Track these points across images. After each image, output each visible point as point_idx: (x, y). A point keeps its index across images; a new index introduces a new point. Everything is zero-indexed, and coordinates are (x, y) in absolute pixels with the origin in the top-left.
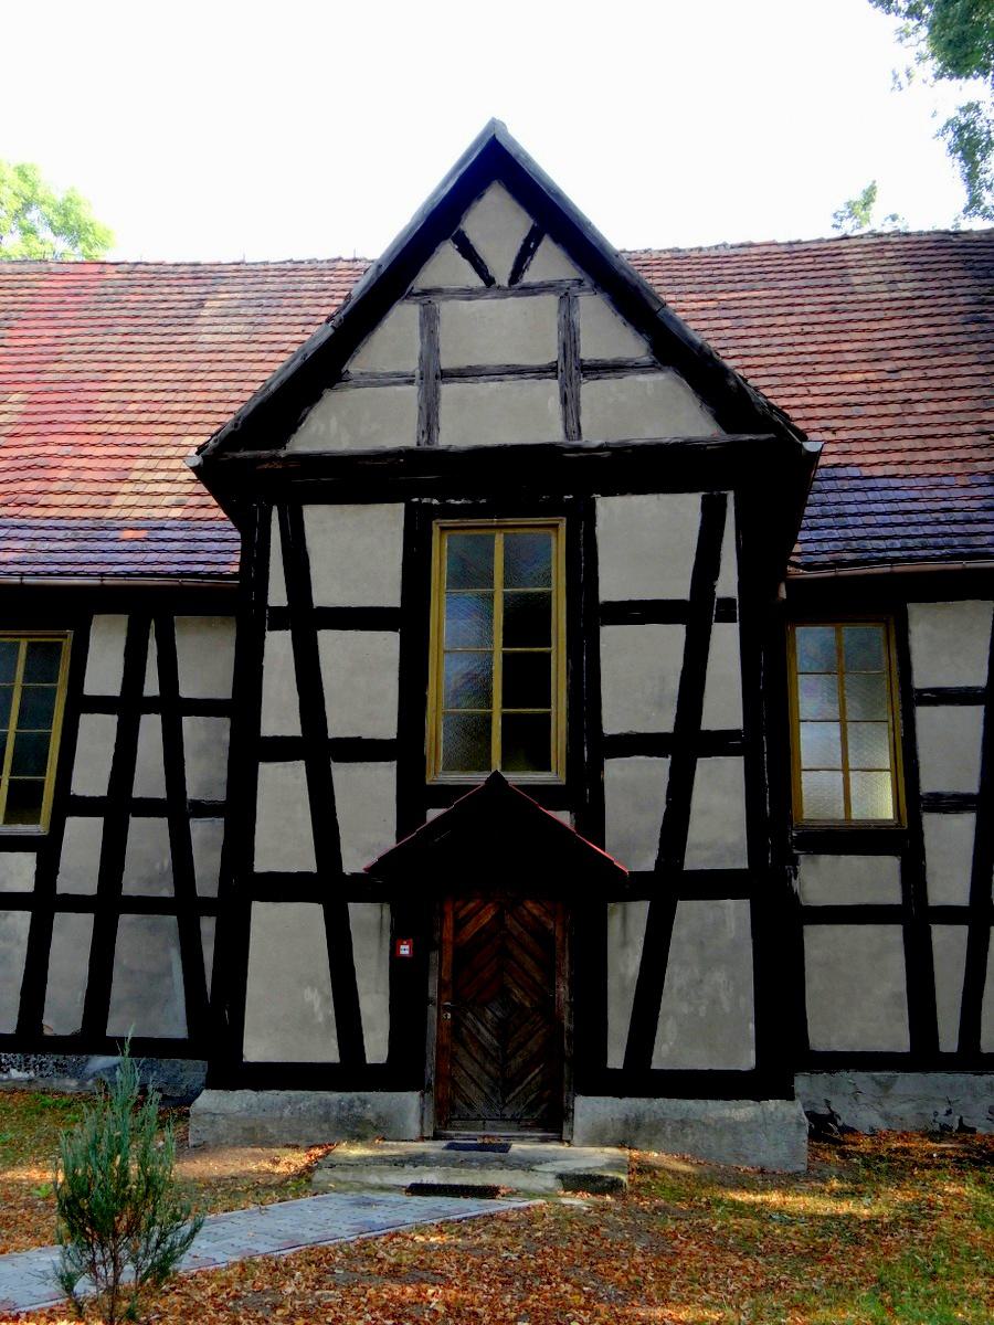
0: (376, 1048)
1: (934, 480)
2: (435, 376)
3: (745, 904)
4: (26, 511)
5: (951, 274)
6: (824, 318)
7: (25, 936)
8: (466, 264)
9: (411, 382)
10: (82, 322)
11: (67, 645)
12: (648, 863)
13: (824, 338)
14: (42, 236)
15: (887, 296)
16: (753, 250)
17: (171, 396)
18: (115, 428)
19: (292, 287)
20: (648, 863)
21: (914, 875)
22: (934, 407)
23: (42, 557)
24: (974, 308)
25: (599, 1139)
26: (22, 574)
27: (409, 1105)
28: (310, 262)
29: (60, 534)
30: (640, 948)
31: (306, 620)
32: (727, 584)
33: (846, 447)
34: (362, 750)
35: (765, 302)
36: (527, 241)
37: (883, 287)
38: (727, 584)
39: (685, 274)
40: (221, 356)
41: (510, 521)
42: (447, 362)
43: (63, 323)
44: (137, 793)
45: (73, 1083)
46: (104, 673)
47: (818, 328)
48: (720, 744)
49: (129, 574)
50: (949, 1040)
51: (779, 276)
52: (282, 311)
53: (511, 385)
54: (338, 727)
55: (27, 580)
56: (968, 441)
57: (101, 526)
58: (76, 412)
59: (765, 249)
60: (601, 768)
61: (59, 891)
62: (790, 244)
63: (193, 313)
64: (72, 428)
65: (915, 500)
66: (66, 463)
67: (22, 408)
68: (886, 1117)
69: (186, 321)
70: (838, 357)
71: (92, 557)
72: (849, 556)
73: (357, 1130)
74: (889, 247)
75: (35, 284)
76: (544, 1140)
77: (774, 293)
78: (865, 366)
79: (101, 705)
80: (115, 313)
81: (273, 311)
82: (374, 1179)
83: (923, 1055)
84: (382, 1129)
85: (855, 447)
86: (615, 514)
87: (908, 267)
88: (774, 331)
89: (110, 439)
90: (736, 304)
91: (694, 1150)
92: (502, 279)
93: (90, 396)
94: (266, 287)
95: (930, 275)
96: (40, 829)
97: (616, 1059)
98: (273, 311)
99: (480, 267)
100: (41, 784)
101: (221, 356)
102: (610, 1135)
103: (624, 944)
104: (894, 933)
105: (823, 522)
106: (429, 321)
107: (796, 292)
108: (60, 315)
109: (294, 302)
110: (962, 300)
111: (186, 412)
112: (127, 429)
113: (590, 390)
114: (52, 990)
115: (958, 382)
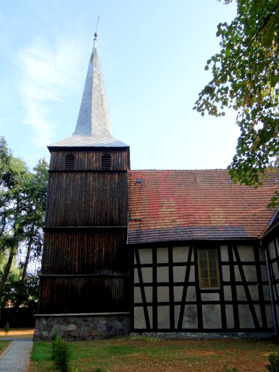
21: (222, 296)
45: (236, 338)
46: (225, 257)
50: (176, 327)
55: (211, 239)
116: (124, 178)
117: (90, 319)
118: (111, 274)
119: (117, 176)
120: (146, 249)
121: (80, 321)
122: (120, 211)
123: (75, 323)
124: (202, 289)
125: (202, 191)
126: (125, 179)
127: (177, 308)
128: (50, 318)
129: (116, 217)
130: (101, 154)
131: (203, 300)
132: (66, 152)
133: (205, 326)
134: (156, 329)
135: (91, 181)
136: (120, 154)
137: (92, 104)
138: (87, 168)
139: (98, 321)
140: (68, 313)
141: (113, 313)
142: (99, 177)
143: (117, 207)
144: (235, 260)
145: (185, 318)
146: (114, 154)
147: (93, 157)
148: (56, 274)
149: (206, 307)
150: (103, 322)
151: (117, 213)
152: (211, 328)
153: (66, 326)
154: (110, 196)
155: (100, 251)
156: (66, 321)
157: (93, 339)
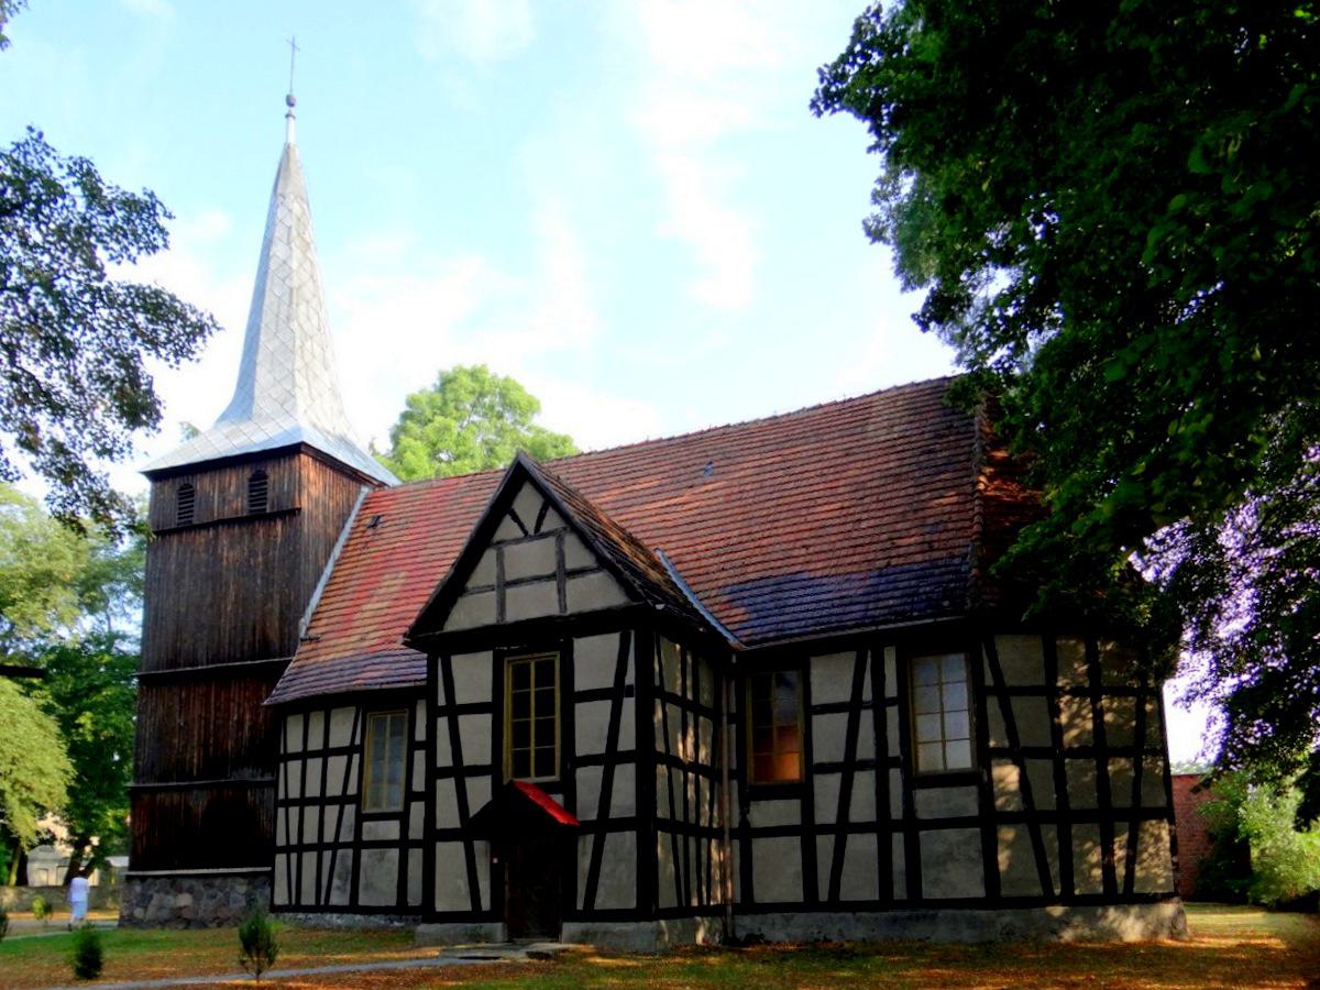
0: (486, 904)
2: (505, 585)
9: (493, 590)
11: (407, 715)
12: (593, 816)
16: (820, 411)
20: (593, 816)
21: (808, 809)
23: (393, 673)
25: (571, 940)
27: (498, 929)
31: (454, 711)
32: (630, 679)
34: (477, 771)
36: (541, 510)
37: (885, 431)
38: (630, 679)
42: (509, 577)
48: (626, 757)
50: (823, 896)
53: (536, 586)
54: (467, 761)
55: (384, 686)
60: (575, 772)
68: (788, 935)
71: (414, 670)
73: (475, 938)
76: (552, 942)
83: (810, 903)
84: (488, 938)
86: (582, 646)
87: (907, 412)
92: (531, 532)
97: (580, 906)
99: (522, 526)
103: (584, 854)
104: (796, 841)
106: (500, 557)
113: (571, 584)
114: (410, 886)
117: (218, 882)
118: (259, 779)
119: (279, 528)
121: (198, 886)
122: (283, 618)
123: (190, 891)
125: (635, 509)
126: (298, 531)
127: (825, 843)
128: (149, 880)
129: (274, 636)
130: (247, 473)
131: (365, 837)
132: (178, 480)
133: (363, 901)
135: (225, 549)
136: (287, 465)
137: (263, 325)
138: (218, 514)
139: (232, 888)
140: (179, 868)
141: (259, 869)
142: (242, 535)
143: (277, 610)
145: (336, 882)
146: (274, 467)
147: (230, 484)
148: (159, 781)
149: (370, 856)
150: (241, 888)
153: (175, 896)
155: (240, 722)
156: (174, 884)
157: (219, 925)
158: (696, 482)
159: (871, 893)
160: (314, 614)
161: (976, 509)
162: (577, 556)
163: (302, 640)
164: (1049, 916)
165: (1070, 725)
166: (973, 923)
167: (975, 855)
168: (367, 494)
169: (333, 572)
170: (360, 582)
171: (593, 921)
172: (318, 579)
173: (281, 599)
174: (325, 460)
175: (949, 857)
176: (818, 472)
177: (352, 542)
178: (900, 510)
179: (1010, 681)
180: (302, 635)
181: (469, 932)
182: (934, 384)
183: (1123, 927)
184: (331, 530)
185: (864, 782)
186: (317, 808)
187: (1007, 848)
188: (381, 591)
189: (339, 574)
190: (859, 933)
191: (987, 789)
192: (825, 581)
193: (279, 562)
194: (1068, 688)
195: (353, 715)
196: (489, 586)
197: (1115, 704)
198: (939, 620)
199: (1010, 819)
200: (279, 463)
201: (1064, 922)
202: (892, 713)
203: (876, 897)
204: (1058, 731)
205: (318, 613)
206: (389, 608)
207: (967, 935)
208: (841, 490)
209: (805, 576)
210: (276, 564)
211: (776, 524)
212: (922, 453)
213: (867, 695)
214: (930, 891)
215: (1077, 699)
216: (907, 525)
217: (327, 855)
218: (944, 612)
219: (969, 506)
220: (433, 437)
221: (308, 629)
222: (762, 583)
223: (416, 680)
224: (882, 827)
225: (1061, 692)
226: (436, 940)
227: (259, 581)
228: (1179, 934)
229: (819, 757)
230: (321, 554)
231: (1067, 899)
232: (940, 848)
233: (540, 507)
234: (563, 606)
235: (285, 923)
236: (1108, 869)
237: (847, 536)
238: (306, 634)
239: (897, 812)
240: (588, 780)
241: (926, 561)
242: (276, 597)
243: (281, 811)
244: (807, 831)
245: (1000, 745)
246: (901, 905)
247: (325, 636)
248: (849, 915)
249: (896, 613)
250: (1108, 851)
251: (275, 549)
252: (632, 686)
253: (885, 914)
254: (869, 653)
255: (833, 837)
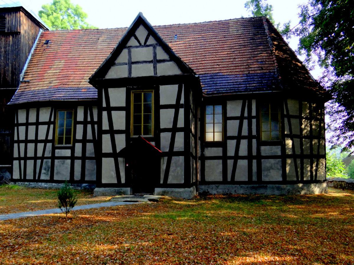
0: (123, 181)
1: (236, 76)
2: (131, 63)
3: (183, 157)
4: (65, 86)
5: (250, 28)
6: (222, 39)
7: (70, 164)
8: (136, 41)
9: (126, 64)
10: (75, 44)
11: (73, 112)
12: (167, 150)
13: (221, 44)
14: (72, 16)
15: (236, 34)
16: (211, 23)
17: (92, 60)
18: (81, 68)
19: (117, 34)
20: (167, 150)
21: (225, 151)
22: (239, 59)
23: (68, 95)
24: (253, 36)
25: (158, 194)
26: (64, 99)
27: (129, 189)
28: (121, 28)
29: (71, 91)
30: (166, 164)
31: (110, 109)
32: (182, 101)
33: (220, 69)
34: (120, 132)
35: (211, 36)
36: (147, 36)
37: (236, 32)
38: (182, 101)
39: (196, 29)
40: (102, 51)
41: (144, 91)
42: (133, 60)
43: (72, 44)
44: (88, 139)
45: (80, 188)
46: (80, 117)
47: (221, 42)
49: (83, 99)
50: (229, 179)
51: (215, 29)
52: (114, 40)
53: (145, 64)
55: (65, 100)
56: (244, 67)
57: (79, 89)
58: (74, 64)
59: (213, 23)
61: (75, 156)
62: (219, 21)
63: (97, 41)
64: (73, 68)
65: (231, 80)
66: (72, 75)
67: (64, 64)
69: (95, 43)
70: (223, 48)
71: (77, 95)
72: (215, 92)
73: (120, 193)
74: (239, 22)
75: (66, 35)
77: (214, 33)
78: (228, 50)
79: (80, 123)
80: (82, 42)
81: (112, 40)
82: (120, 200)
83: (225, 181)
84: (124, 193)
85: (222, 69)
86: (163, 89)
87: (242, 27)
88: (212, 42)
89: (80, 70)
90: (205, 36)
91: (174, 196)
92: (143, 44)
93: (77, 61)
94: (112, 34)
95: (246, 28)
96: (71, 145)
97: (162, 182)
98: (112, 40)
100: (71, 137)
101: (102, 51)
102: (160, 194)
103: (163, 164)
105: (213, 85)
106: (130, 52)
107: (218, 33)
108: (71, 42)
109: (117, 38)
110: (251, 34)
111: (95, 64)
112: (84, 68)
113: (159, 65)
114: (75, 173)
115: (246, 54)
116: (18, 40)
120: (23, 110)
122: (13, 73)
124: (57, 145)
126: (19, 41)
127: (230, 162)
129: (9, 78)
131: (56, 155)
133: (56, 178)
134: (25, 180)
136: (14, 14)
143: (10, 69)
144: (89, 119)
145: (43, 171)
151: (10, 75)
152: (60, 179)
154: (4, 59)
158: (172, 41)
159: (245, 178)
160: (25, 73)
161: (274, 58)
162: (161, 54)
163: (21, 82)
164: (298, 186)
165: (305, 129)
166: (278, 189)
167: (279, 167)
168: (42, 32)
169: (31, 58)
170: (44, 63)
171: (167, 187)
172: (26, 60)
173: (12, 66)
174: (29, 16)
175: (271, 168)
176: (216, 42)
177: (38, 48)
178: (248, 56)
179: (291, 113)
180: (21, 80)
181: (117, 191)
182: (249, 19)
183: (315, 190)
184: (30, 42)
185: (244, 143)
186: (34, 144)
187: (289, 165)
188: (55, 66)
189: (34, 59)
190: (241, 191)
191: (284, 147)
192: (228, 76)
193: (11, 52)
194: (304, 117)
195: (50, 113)
196: (125, 63)
197: (315, 123)
198: (254, 92)
199: (289, 156)
200: (11, 14)
201: (302, 189)
202: (254, 121)
203: (247, 180)
204: (302, 130)
205: (27, 73)
206: (60, 72)
207: (277, 192)
208: (226, 48)
209: (221, 74)
210: (10, 52)
211: (205, 57)
212: (251, 40)
213: (246, 115)
214: (264, 179)
215: (306, 121)
216: (252, 61)
217: (39, 162)
218: (274, 89)
219: (271, 57)
220: (53, 20)
221: (23, 78)
222: (206, 75)
223: (78, 99)
224: (249, 157)
225: (303, 118)
226: (103, 194)
227: (2, 58)
228: (327, 192)
229: (229, 134)
230: (27, 51)
231: (302, 181)
232: (268, 165)
233: (147, 35)
234: (155, 73)
235: (19, 186)
236: (311, 172)
237: (232, 63)
238: (22, 80)
239: (254, 153)
240: (165, 137)
241: (262, 73)
242: (10, 65)
243: (16, 145)
244: (224, 158)
245: (288, 133)
246: (255, 183)
247: (31, 81)
248: (238, 186)
249: (257, 88)
250: (312, 168)
251: (9, 46)
252: (182, 104)
253: (250, 185)
254: (247, 101)
255: (233, 160)
